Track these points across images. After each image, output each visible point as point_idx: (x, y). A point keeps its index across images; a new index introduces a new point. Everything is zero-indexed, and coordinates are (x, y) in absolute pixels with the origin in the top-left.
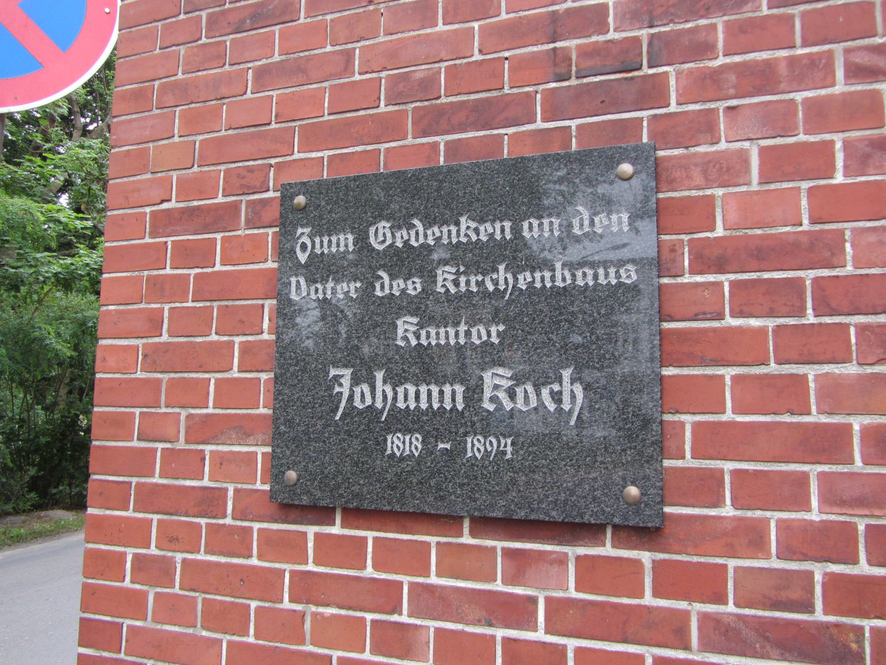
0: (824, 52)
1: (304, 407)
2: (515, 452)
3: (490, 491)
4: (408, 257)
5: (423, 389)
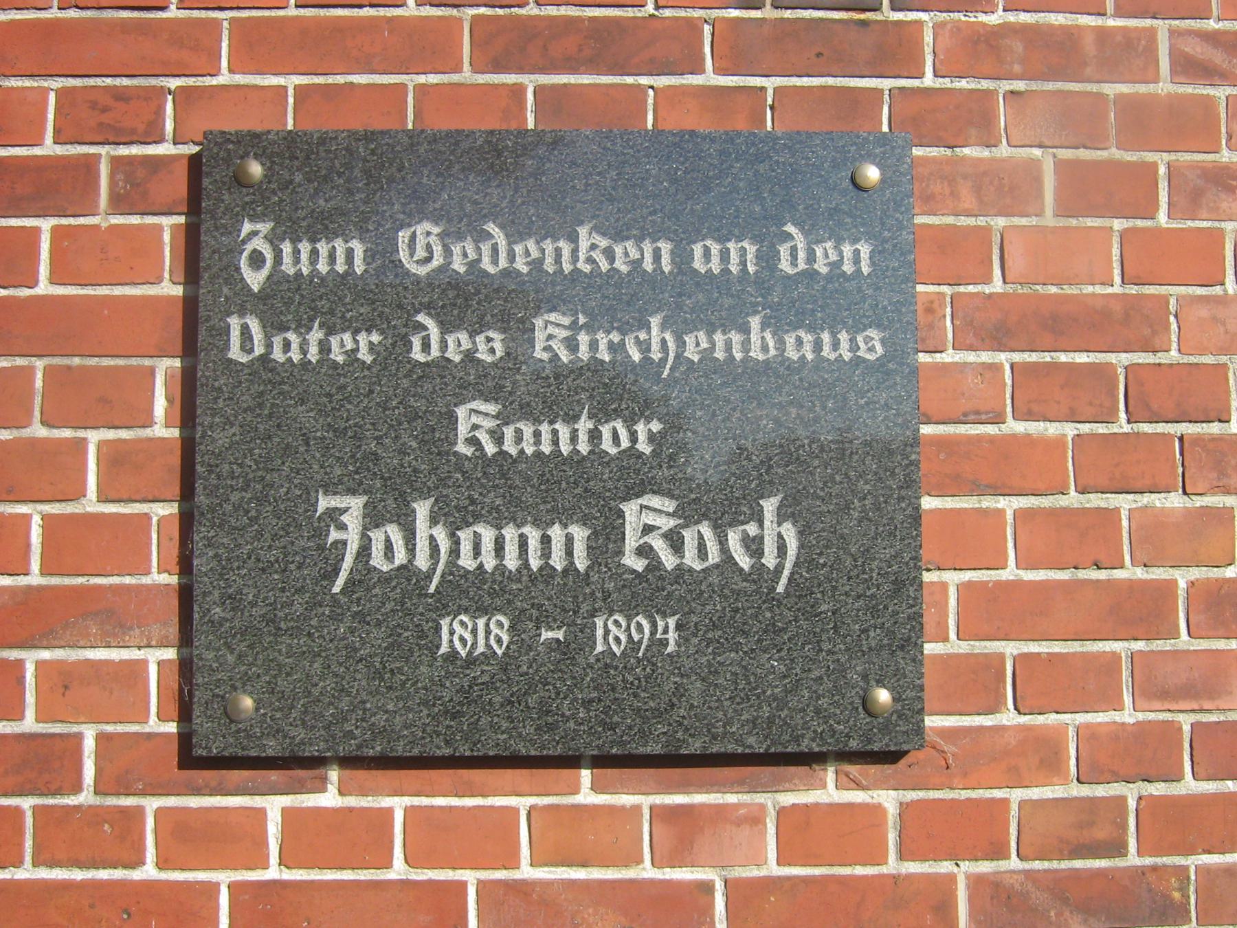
0: (1144, 29)
1: (263, 570)
2: (683, 641)
3: (639, 710)
4: (478, 292)
5: (510, 533)
